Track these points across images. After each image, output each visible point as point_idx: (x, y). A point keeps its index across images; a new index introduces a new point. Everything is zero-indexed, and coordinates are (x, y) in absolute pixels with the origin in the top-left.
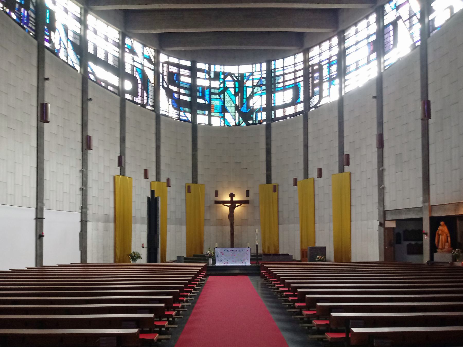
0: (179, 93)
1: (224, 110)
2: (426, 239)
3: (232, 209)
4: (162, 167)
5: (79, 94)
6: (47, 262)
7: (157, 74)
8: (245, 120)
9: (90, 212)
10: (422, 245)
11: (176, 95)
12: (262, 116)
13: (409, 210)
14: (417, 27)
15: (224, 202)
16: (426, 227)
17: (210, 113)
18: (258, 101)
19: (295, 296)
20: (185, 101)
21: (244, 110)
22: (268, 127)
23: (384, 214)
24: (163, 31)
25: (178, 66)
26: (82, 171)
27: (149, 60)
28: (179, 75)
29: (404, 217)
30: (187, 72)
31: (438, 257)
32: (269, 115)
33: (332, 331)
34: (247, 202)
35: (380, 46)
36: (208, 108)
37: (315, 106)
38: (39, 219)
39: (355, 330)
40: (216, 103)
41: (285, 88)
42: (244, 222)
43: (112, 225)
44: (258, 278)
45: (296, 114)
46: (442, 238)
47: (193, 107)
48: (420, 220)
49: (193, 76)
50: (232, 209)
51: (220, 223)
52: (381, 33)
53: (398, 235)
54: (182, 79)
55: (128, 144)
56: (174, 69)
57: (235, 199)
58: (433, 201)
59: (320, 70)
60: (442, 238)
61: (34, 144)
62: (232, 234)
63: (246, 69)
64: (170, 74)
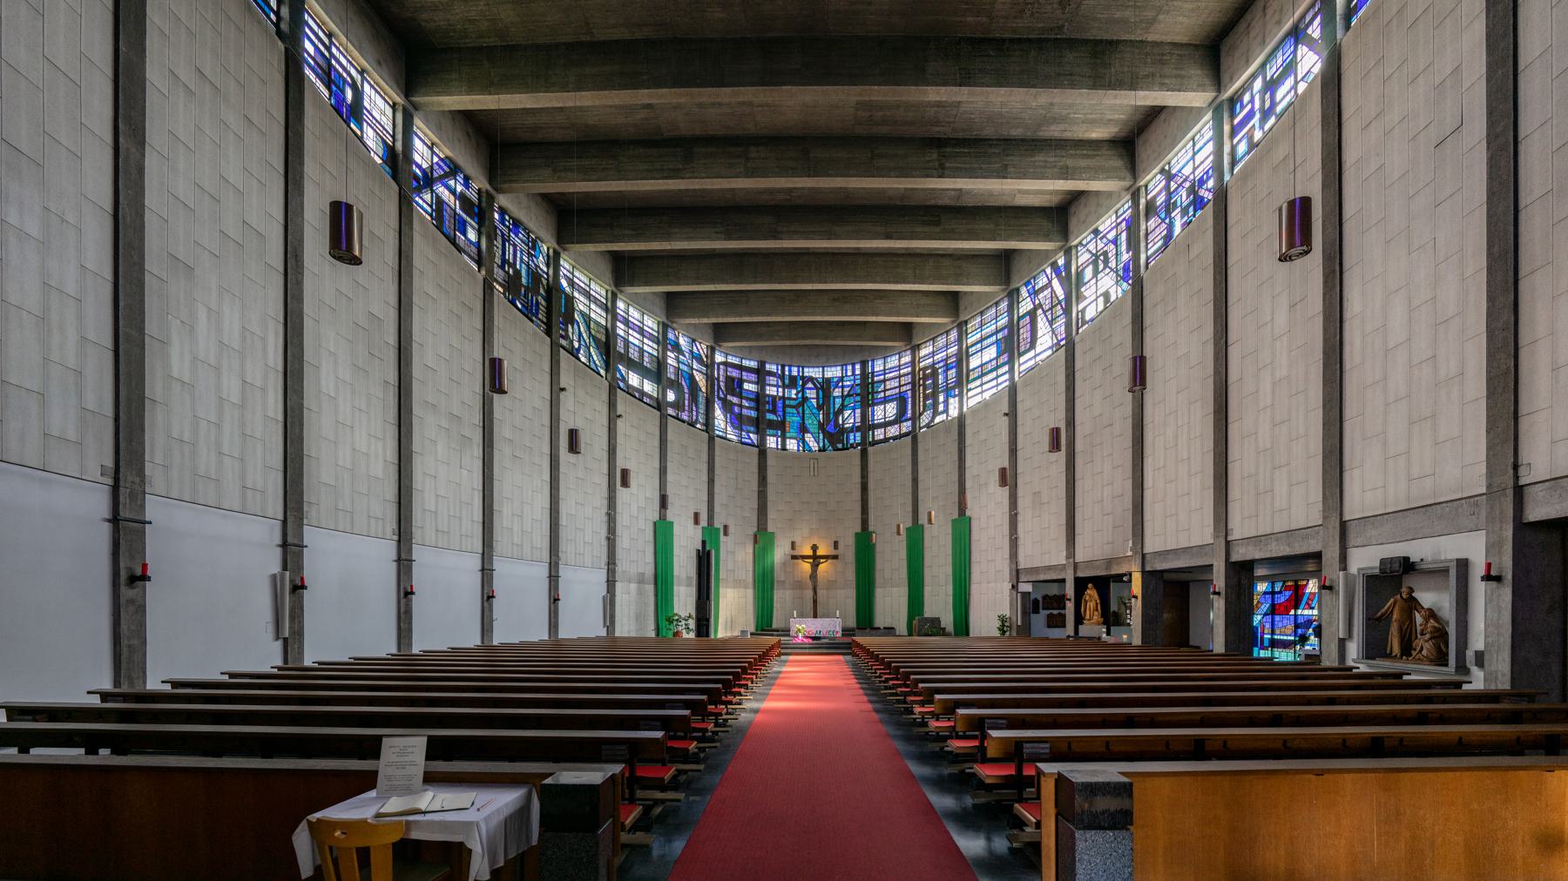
0: (741, 406)
1: (803, 429)
2: (1070, 606)
3: (815, 566)
4: (717, 509)
5: (606, 409)
6: (564, 634)
7: (710, 379)
8: (833, 444)
9: (619, 569)
10: (1064, 616)
11: (736, 409)
12: (855, 438)
13: (1049, 568)
14: (1060, 324)
15: (804, 557)
16: (1070, 590)
17: (784, 432)
18: (850, 418)
19: (915, 694)
20: (749, 418)
21: (830, 428)
22: (864, 453)
23: (1017, 574)
24: (720, 320)
25: (741, 368)
26: (609, 515)
27: (699, 359)
28: (741, 382)
29: (1042, 577)
30: (753, 377)
31: (1085, 630)
32: (864, 437)
33: (958, 737)
34: (835, 557)
35: (1010, 346)
36: (781, 427)
37: (928, 426)
38: (553, 578)
39: (994, 733)
40: (793, 419)
41: (885, 401)
42: (831, 585)
43: (650, 588)
44: (849, 658)
45: (901, 436)
46: (1091, 605)
47: (760, 426)
48: (1063, 581)
49: (761, 383)
50: (815, 566)
51: (799, 585)
52: (1012, 328)
53: (1036, 602)
54: (746, 386)
55: (670, 477)
56: (735, 373)
57: (820, 552)
58: (1080, 557)
59: (935, 374)
60: (1091, 605)
61: (547, 477)
62: (815, 601)
63: (833, 372)
64: (729, 380)
